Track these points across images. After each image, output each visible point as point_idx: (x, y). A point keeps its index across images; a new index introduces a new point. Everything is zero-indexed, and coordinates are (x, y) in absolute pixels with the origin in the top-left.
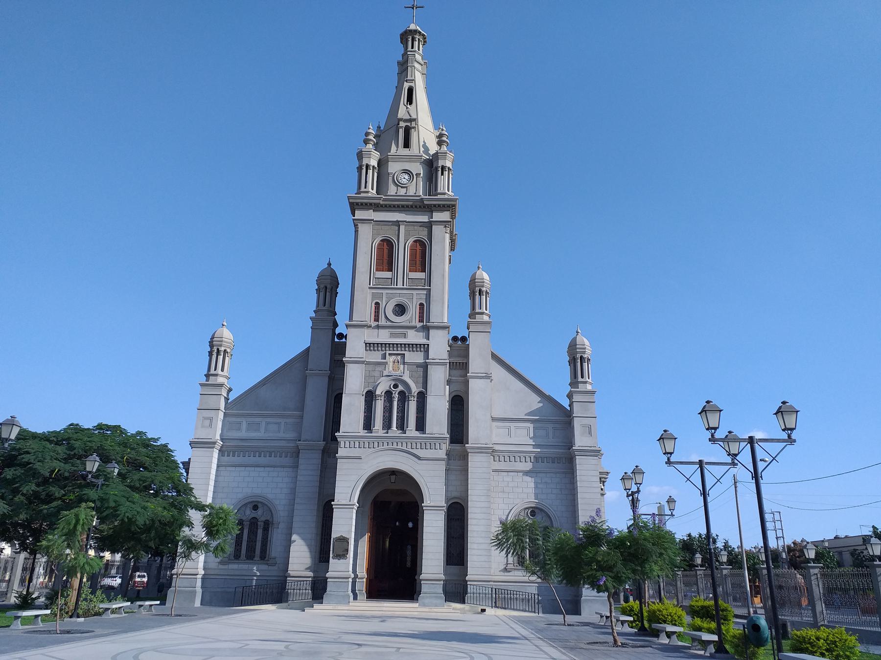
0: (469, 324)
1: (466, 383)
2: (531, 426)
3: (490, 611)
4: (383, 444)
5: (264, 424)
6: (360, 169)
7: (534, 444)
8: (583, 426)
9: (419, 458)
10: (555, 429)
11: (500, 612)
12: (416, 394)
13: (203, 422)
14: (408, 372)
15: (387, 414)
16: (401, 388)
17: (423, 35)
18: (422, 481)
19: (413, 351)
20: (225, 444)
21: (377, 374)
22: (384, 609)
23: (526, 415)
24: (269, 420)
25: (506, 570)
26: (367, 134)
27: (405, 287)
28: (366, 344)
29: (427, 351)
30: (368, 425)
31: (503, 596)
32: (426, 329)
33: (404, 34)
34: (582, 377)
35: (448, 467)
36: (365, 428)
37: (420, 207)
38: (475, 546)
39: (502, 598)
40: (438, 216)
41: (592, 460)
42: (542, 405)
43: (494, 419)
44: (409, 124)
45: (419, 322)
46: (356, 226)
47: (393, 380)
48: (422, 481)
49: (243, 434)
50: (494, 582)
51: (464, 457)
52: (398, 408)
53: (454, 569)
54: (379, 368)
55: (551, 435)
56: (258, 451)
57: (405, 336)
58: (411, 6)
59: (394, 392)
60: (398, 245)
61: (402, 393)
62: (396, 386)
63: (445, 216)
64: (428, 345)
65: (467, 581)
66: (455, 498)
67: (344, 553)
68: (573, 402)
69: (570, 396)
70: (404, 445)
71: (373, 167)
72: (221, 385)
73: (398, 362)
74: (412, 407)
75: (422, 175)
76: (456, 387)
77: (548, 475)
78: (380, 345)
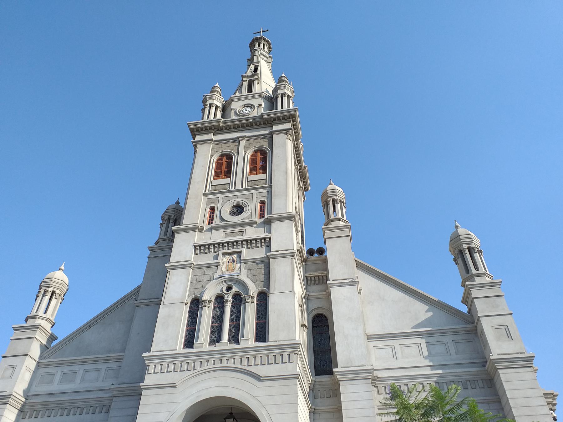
0: (325, 231)
2: (423, 342)
7: (431, 364)
8: (496, 327)
9: (258, 378)
10: (456, 341)
12: (256, 295)
13: (4, 371)
14: (246, 270)
16: (235, 289)
17: (267, 41)
18: (264, 412)
19: (252, 248)
20: (28, 401)
21: (206, 278)
23: (412, 328)
24: (87, 367)
28: (195, 247)
29: (269, 246)
30: (189, 342)
32: (268, 223)
33: (252, 42)
37: (260, 124)
41: (525, 374)
42: (430, 314)
43: (370, 338)
45: (260, 218)
46: (195, 148)
48: (264, 412)
49: (55, 387)
51: (335, 393)
52: (231, 316)
54: (210, 271)
55: (453, 350)
57: (242, 233)
59: (226, 296)
60: (238, 156)
62: (229, 289)
64: (270, 238)
73: (234, 262)
75: (263, 106)
76: (315, 304)
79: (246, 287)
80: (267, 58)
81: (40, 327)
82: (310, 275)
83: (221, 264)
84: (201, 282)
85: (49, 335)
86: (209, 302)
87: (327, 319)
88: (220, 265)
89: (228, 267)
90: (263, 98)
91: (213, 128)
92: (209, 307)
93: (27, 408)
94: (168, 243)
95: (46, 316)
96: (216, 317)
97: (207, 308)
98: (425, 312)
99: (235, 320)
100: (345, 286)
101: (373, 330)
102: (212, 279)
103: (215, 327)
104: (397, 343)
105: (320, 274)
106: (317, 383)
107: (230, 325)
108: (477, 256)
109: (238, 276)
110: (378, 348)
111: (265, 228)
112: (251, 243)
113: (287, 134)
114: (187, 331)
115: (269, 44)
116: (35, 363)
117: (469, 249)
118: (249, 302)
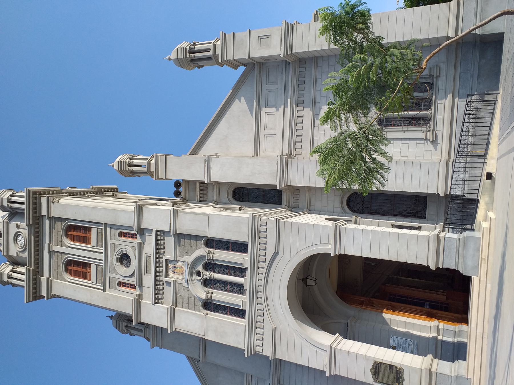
1: (219, 184)
2: (264, 110)
3: (491, 166)
4: (260, 298)
7: (283, 107)
9: (276, 254)
10: (267, 82)
11: (493, 150)
14: (184, 256)
16: (200, 268)
18: (303, 252)
19: (164, 248)
21: (186, 295)
22: (480, 330)
23: (253, 117)
25: (434, 142)
28: (155, 303)
29: (164, 233)
31: (470, 138)
32: (142, 231)
35: (305, 210)
38: (399, 182)
39: (474, 139)
41: (298, 31)
42: (243, 99)
43: (256, 154)
45: (136, 238)
46: (54, 296)
47: (191, 276)
48: (303, 252)
50: (449, 157)
51: (296, 190)
52: (223, 273)
53: (431, 210)
55: (272, 86)
59: (205, 277)
60: (69, 254)
62: (199, 273)
64: (157, 231)
65: (446, 195)
66: (342, 200)
67: (394, 372)
68: (233, 59)
71: (12, 271)
73: (175, 267)
75: (18, 223)
77: (318, 89)
78: (157, 287)
86: (208, 292)
91: (35, 277)
97: (213, 295)
99: (226, 270)
100: (211, 168)
101: (250, 150)
102: (188, 289)
105: (199, 188)
106: (287, 204)
107: (231, 275)
108: (197, 47)
109: (188, 264)
111: (147, 234)
114: (230, 314)
117: (191, 52)
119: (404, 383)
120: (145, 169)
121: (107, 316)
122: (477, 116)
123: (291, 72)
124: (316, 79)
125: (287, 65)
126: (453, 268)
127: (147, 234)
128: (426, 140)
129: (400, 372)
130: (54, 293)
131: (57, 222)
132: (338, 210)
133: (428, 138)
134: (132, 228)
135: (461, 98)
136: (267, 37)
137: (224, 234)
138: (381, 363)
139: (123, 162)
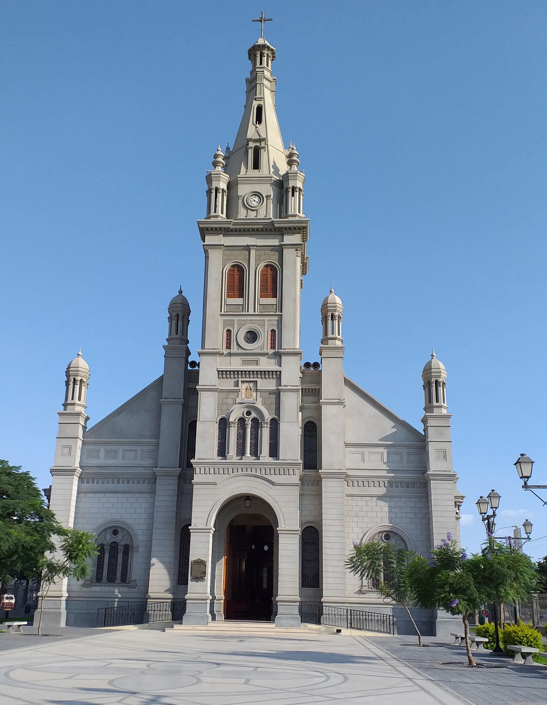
2: (385, 451)
3: (345, 632)
5: (121, 450)
6: (209, 192)
7: (388, 468)
8: (438, 450)
9: (273, 484)
10: (409, 453)
11: (356, 633)
12: (269, 421)
14: (261, 399)
15: (241, 441)
16: (254, 415)
18: (277, 505)
20: (84, 471)
21: (230, 401)
22: (242, 629)
23: (379, 440)
25: (360, 592)
26: (216, 156)
27: (256, 313)
28: (219, 371)
29: (279, 378)
30: (222, 451)
32: (278, 356)
33: (252, 49)
34: (437, 401)
35: (302, 492)
36: (219, 455)
37: (271, 230)
38: (330, 569)
40: (289, 239)
41: (447, 485)
42: (395, 430)
43: (347, 445)
44: (258, 144)
45: (271, 348)
46: (206, 252)
47: (246, 407)
48: (277, 505)
49: (101, 461)
51: (318, 482)
52: (251, 435)
53: (309, 591)
55: (405, 460)
56: (116, 478)
57: (257, 363)
58: (259, 19)
59: (247, 419)
60: (249, 270)
61: (255, 420)
62: (249, 413)
63: (296, 239)
64: (280, 372)
68: (428, 426)
69: (424, 421)
70: (258, 470)
71: (223, 190)
72: (79, 414)
73: (251, 389)
74: (265, 433)
75: (272, 197)
79: (262, 416)
80: (271, 82)
81: (82, 414)
82: (305, 388)
83: (241, 391)
84: (226, 405)
85: (85, 418)
86: (234, 423)
87: (316, 426)
88: (240, 391)
89: (247, 394)
90: (272, 184)
91: (223, 230)
92: (234, 427)
93: (83, 476)
94: (181, 344)
95: (81, 402)
96: (240, 435)
97: (233, 427)
98: (391, 428)
99: (254, 439)
100: (334, 405)
101: (350, 439)
102: (235, 403)
103: (240, 443)
104: (366, 450)
105: (314, 388)
106: (305, 475)
107: (251, 443)
108: (440, 389)
109: (254, 403)
110: (352, 453)
111: (276, 360)
112: (265, 374)
113: (297, 250)
114: (219, 443)
115: (273, 53)
116: (81, 441)
117: (436, 382)
118: (264, 427)
119: (195, 582)
120: (330, 335)
121: (181, 286)
122: (373, 621)
123: (416, 475)
124: (410, 497)
125: (422, 472)
126: (278, 612)
127: (276, 360)
128: (362, 586)
129: (202, 579)
130: (210, 251)
131: (278, 253)
132: (304, 519)
133: (363, 587)
134: (280, 347)
135: (392, 610)
136: (445, 458)
137: (216, 280)
138: (206, 566)
139: (335, 308)
